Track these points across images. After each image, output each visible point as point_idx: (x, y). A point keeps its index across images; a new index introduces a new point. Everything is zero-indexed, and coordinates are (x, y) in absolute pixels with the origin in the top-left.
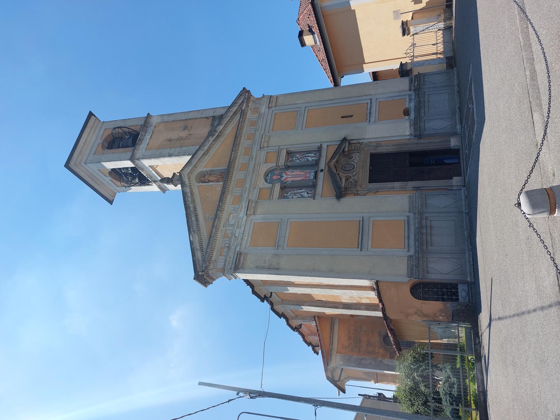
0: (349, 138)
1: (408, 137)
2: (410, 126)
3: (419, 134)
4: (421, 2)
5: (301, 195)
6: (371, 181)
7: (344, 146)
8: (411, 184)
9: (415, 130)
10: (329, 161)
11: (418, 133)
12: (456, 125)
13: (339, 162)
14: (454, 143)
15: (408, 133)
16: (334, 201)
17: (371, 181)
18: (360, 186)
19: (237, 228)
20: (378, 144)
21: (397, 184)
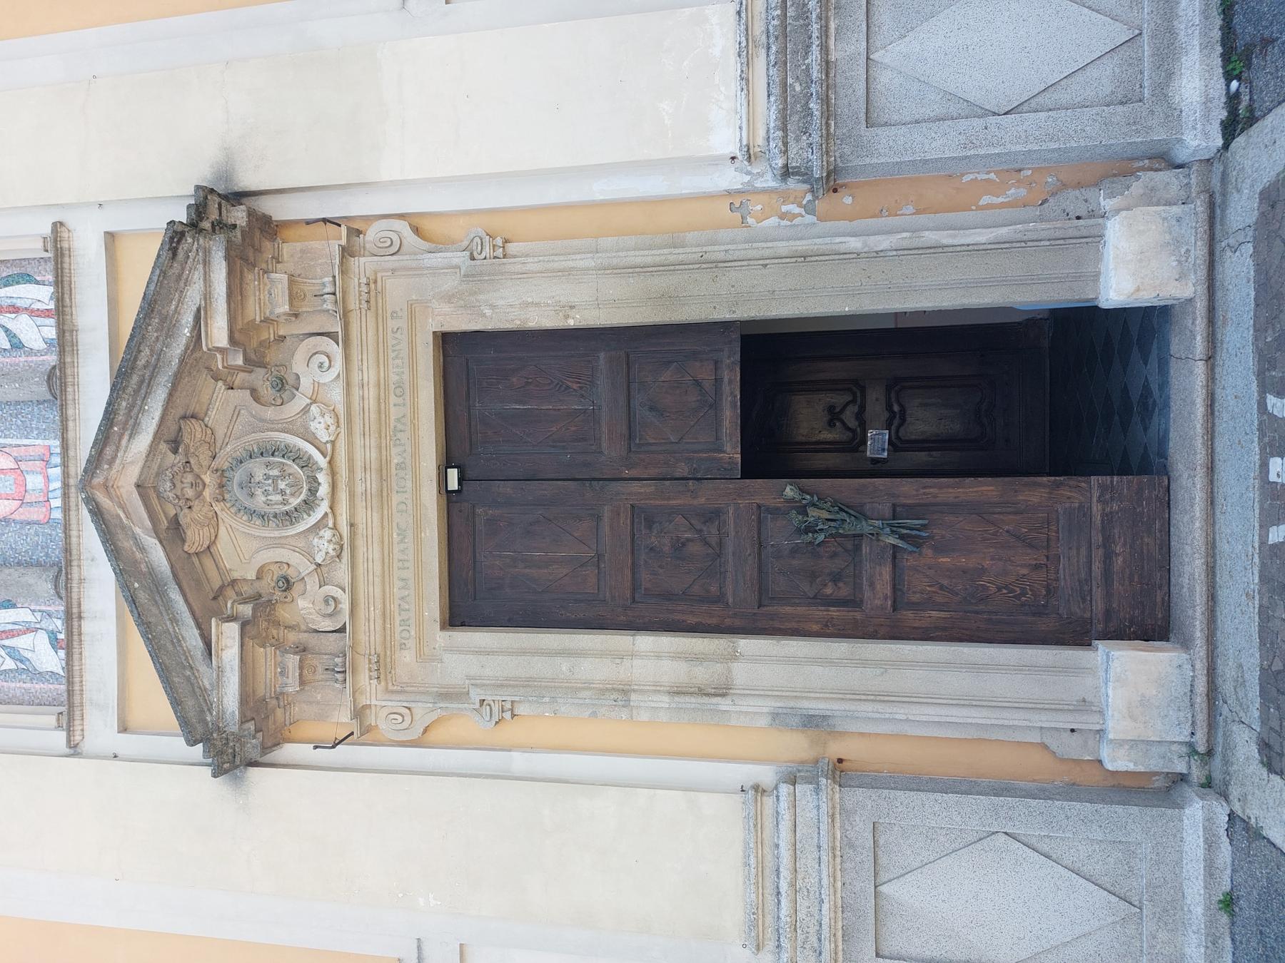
0: (248, 180)
1: (731, 179)
2: (745, 55)
3: (820, 133)
4: (1274, 758)
5: (13, 653)
6: (459, 615)
7: (193, 295)
8: (770, 666)
9: (790, 115)
10: (95, 462)
11: (805, 153)
12: (1167, 56)
13: (193, 432)
14: (1131, 263)
15: (726, 140)
16: (200, 782)
17: (459, 615)
18: (381, 668)
19: (17, 460)
20: (492, 246)
21: (653, 657)
